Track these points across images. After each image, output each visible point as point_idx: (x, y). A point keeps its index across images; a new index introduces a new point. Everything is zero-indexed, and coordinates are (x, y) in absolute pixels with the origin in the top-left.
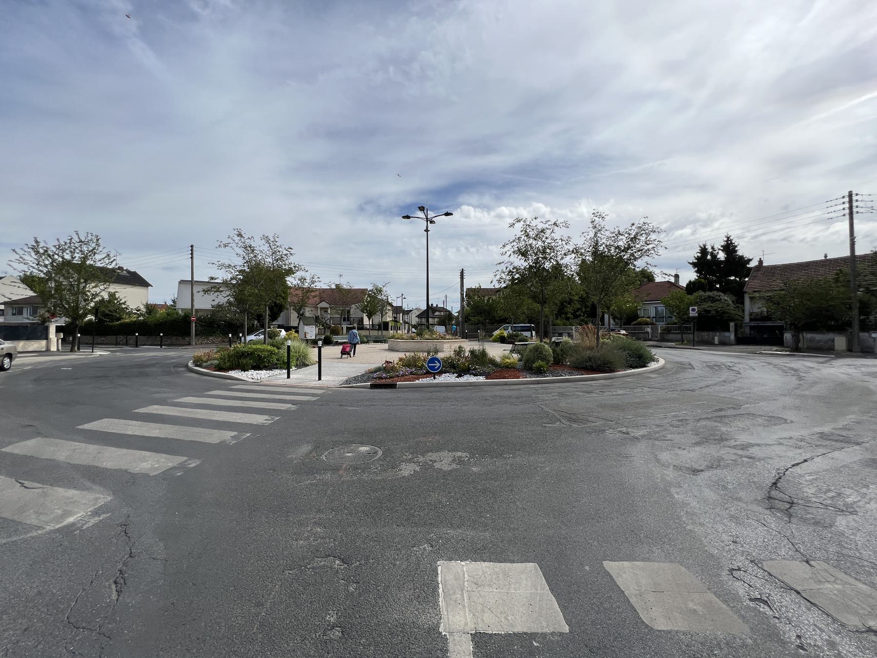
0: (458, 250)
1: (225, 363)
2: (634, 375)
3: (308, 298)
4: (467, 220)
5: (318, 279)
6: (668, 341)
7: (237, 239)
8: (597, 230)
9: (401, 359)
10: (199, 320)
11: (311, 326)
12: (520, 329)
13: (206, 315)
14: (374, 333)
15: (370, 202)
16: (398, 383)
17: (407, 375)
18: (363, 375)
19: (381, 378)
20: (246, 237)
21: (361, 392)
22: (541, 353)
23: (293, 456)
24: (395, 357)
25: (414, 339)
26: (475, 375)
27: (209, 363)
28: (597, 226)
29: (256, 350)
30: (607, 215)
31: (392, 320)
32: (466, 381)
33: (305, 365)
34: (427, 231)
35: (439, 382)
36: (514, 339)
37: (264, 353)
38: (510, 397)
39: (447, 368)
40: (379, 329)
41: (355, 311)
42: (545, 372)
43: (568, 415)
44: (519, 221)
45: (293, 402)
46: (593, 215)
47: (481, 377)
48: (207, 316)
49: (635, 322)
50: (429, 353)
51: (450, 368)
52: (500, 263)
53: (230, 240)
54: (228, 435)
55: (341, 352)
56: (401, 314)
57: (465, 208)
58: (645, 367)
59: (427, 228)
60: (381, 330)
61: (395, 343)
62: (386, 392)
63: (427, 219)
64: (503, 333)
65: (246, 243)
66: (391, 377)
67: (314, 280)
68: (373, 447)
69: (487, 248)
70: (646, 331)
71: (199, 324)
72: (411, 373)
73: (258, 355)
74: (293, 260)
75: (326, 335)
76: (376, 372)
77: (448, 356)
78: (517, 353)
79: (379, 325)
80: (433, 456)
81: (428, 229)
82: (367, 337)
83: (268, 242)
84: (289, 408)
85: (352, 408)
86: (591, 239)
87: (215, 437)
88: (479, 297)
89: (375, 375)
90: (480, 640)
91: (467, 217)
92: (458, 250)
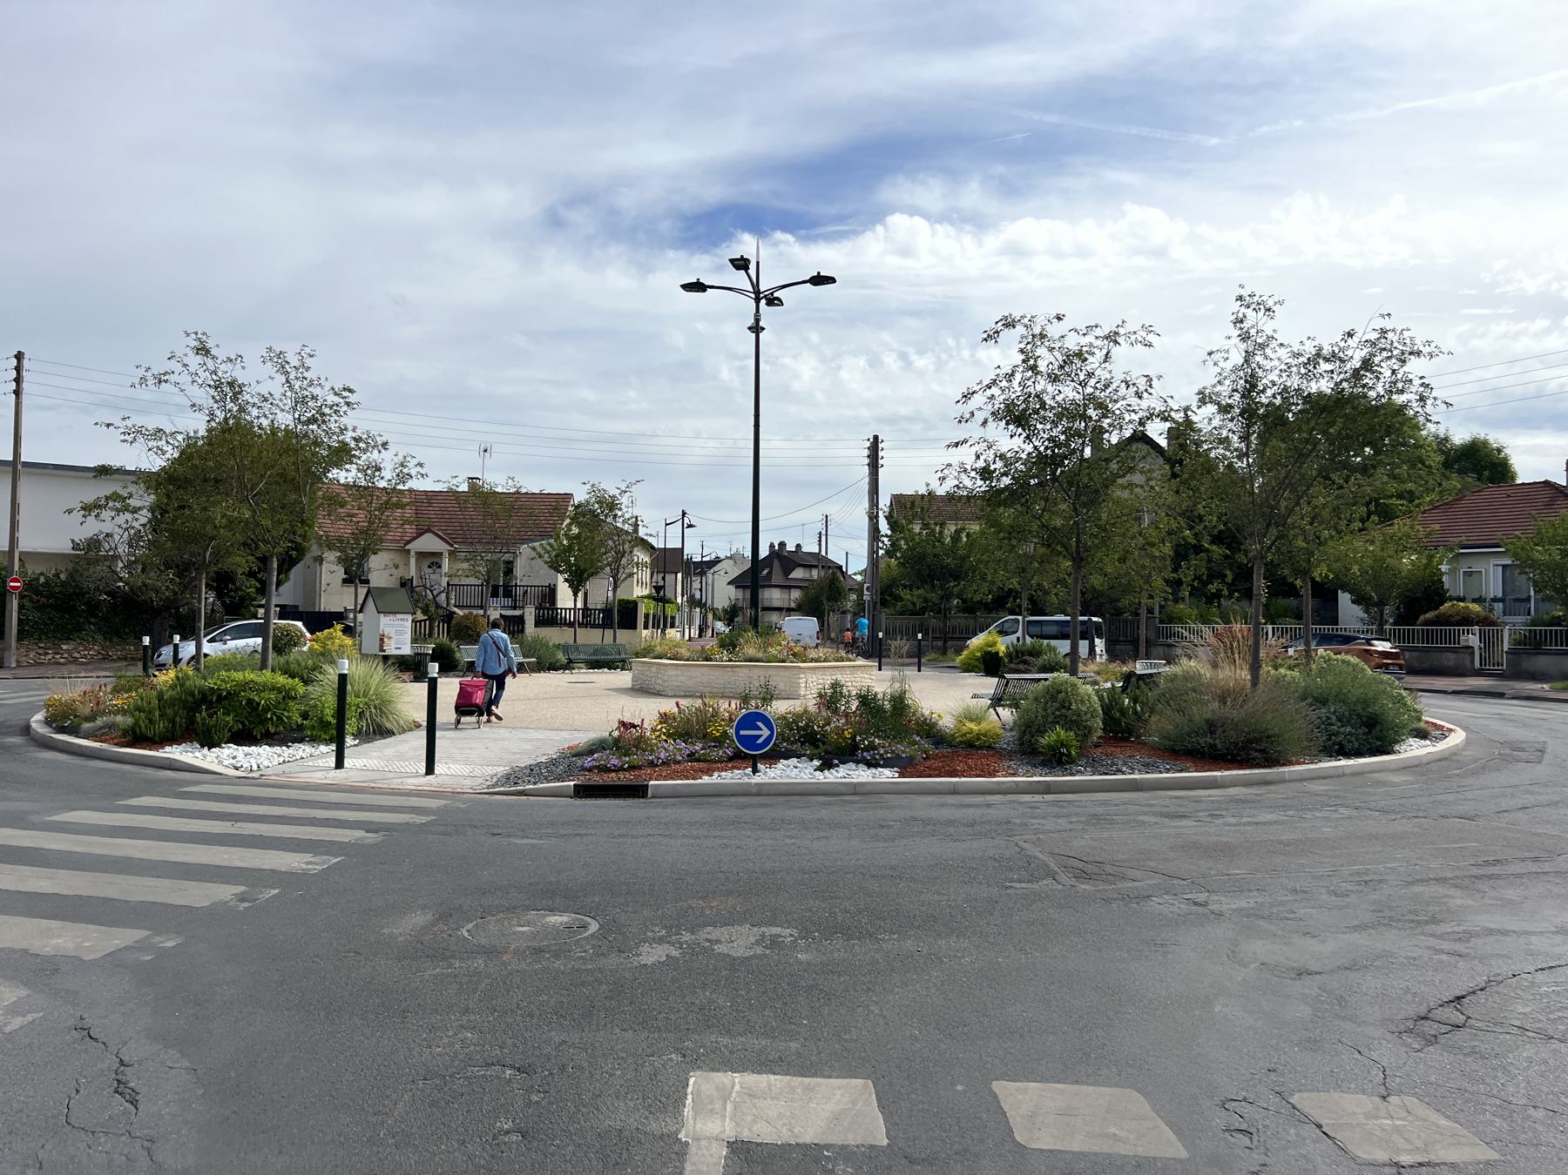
0: (875, 362)
1: (151, 721)
2: (1344, 775)
3: (387, 526)
4: (909, 262)
5: (419, 469)
6: (1534, 677)
7: (194, 361)
8: (1254, 344)
9: (664, 718)
10: (31, 586)
11: (399, 616)
12: (1053, 630)
13: (53, 572)
14: (591, 637)
15: (583, 197)
16: (652, 783)
17: (679, 762)
18: (553, 762)
19: (605, 769)
20: (222, 356)
21: (548, 806)
22: (1066, 705)
23: (395, 931)
24: (647, 712)
25: (711, 660)
26: (870, 765)
27: (99, 722)
28: (1253, 332)
29: (245, 686)
30: (1280, 303)
31: (649, 597)
32: (844, 780)
33: (383, 732)
34: (756, 329)
35: (767, 781)
36: (1025, 662)
37: (266, 695)
38: (951, 823)
39: (792, 743)
40: (607, 624)
41: (530, 567)
42: (1072, 761)
43: (1080, 865)
44: (1010, 324)
45: (369, 827)
46: (1239, 303)
47: (887, 772)
48: (57, 575)
49: (1430, 615)
50: (745, 699)
51: (803, 743)
52: (957, 445)
53: (174, 366)
54: (225, 892)
55: (457, 708)
56: (679, 575)
57: (898, 220)
58: (1389, 753)
59: (757, 320)
60: (611, 627)
61: (654, 669)
62: (617, 805)
63: (757, 292)
64: (994, 644)
65: (220, 374)
66: (632, 768)
67: (405, 471)
68: (578, 916)
69: (973, 356)
70: (1463, 644)
71: (31, 600)
72: (692, 757)
73: (250, 701)
74: (356, 422)
75: (437, 641)
76: (591, 752)
77: (799, 709)
78: (1010, 706)
79: (607, 611)
80: (716, 933)
81: (761, 324)
82: (565, 648)
83: (283, 369)
84: (360, 839)
85: (525, 841)
86: (1235, 369)
87: (199, 895)
88: (925, 526)
89: (588, 762)
90: (740, 1150)
91: (906, 252)
92: (875, 362)
